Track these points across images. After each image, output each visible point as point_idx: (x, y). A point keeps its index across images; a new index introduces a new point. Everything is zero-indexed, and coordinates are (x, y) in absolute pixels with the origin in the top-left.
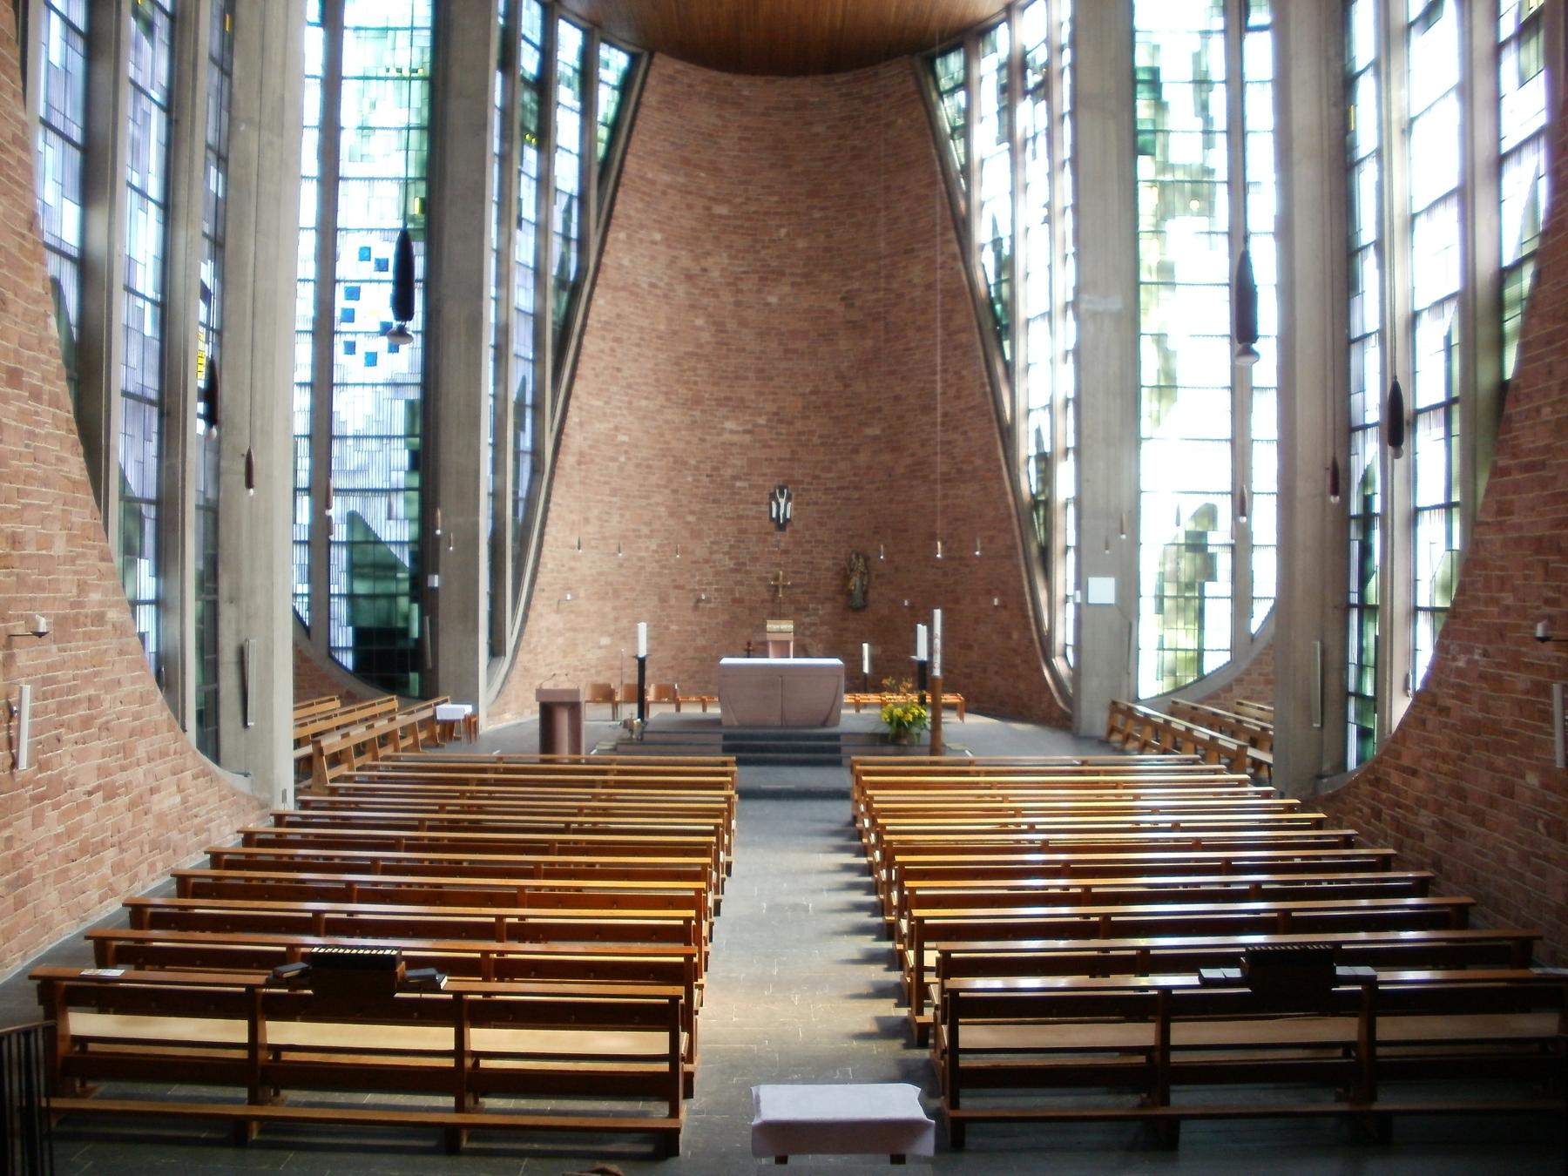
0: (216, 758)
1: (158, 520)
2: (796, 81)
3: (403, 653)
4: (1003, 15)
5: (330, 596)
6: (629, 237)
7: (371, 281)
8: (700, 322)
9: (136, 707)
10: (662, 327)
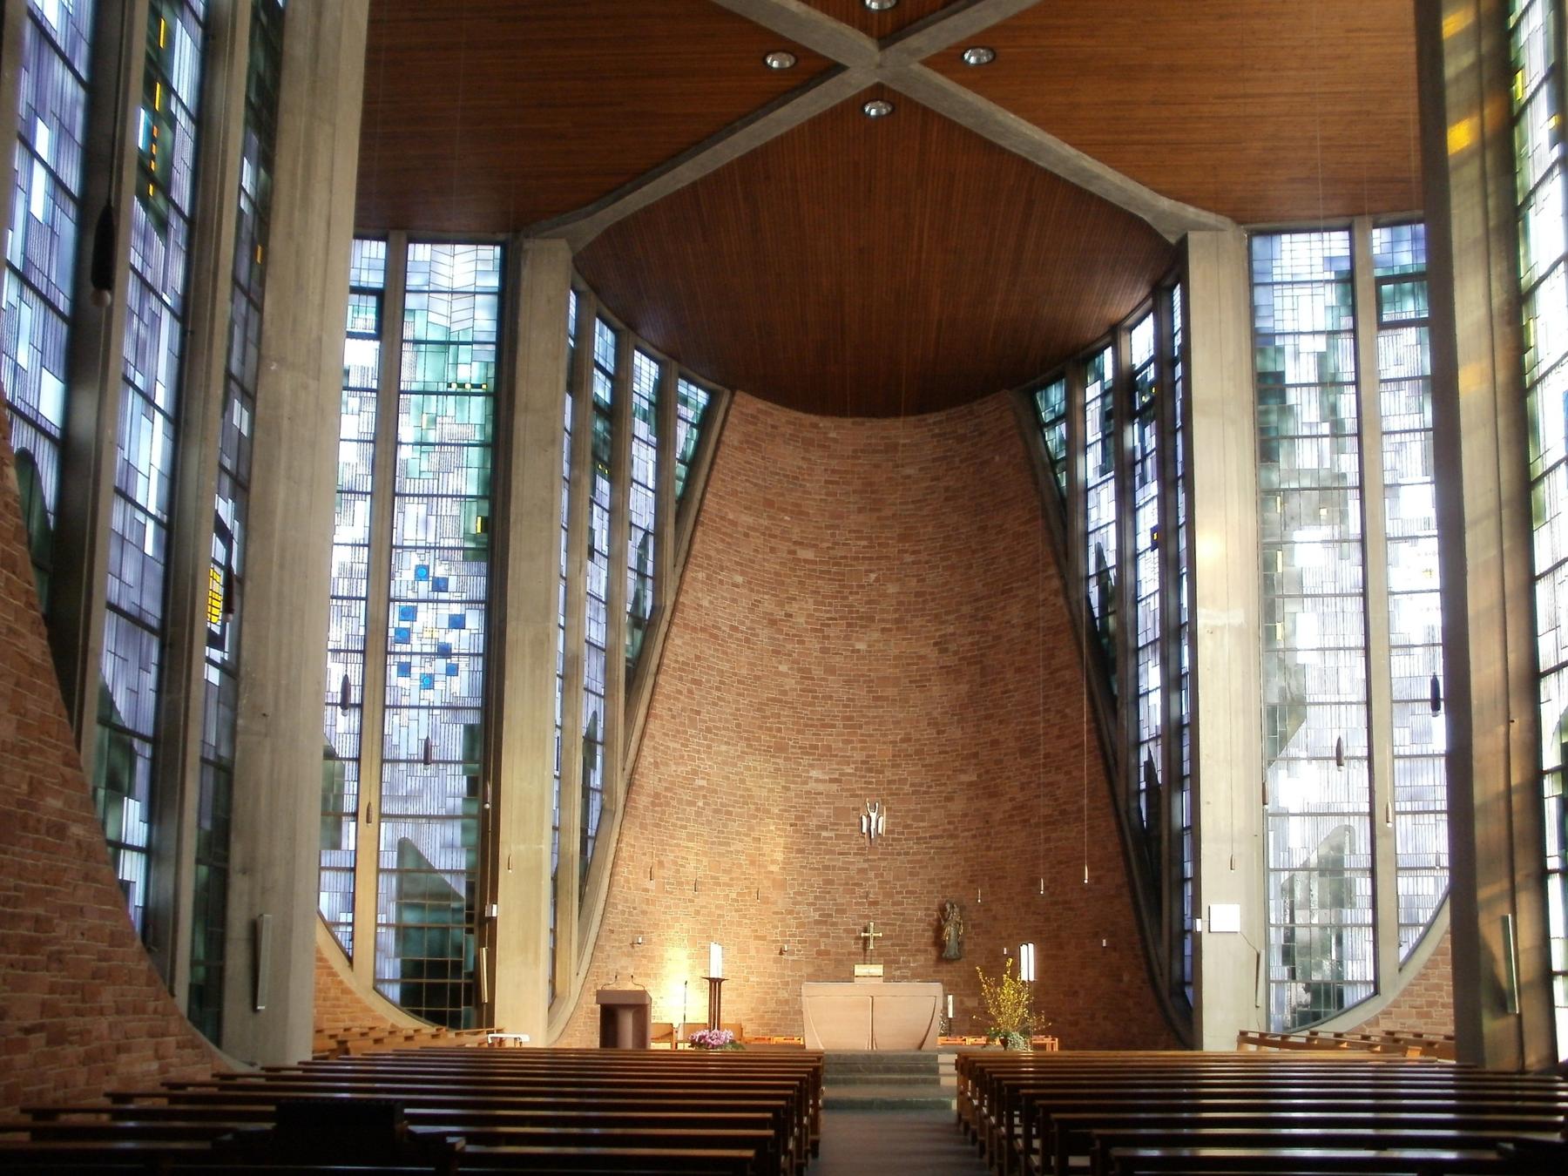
0: (218, 1041)
1: (154, 760)
2: (887, 422)
4: (1108, 339)
6: (709, 577)
8: (783, 668)
9: (103, 946)
10: (744, 672)
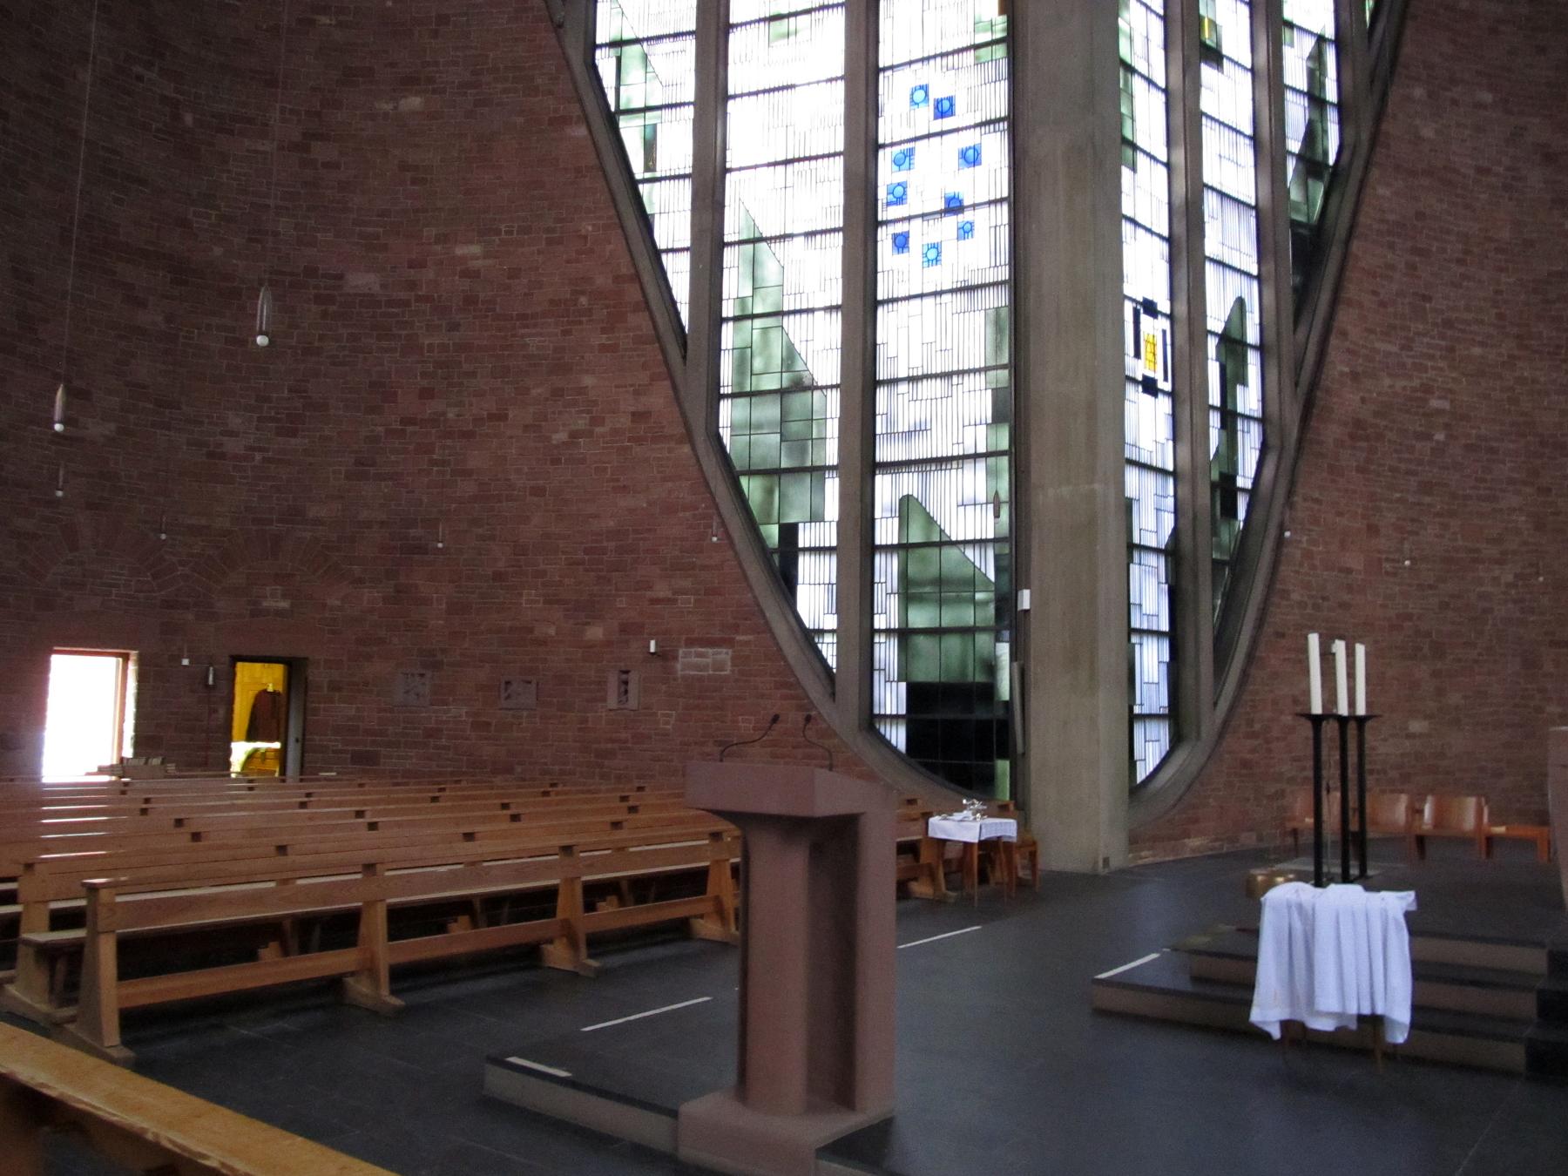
3: (985, 726)
5: (874, 632)
7: (929, 136)
10: (1505, 234)
